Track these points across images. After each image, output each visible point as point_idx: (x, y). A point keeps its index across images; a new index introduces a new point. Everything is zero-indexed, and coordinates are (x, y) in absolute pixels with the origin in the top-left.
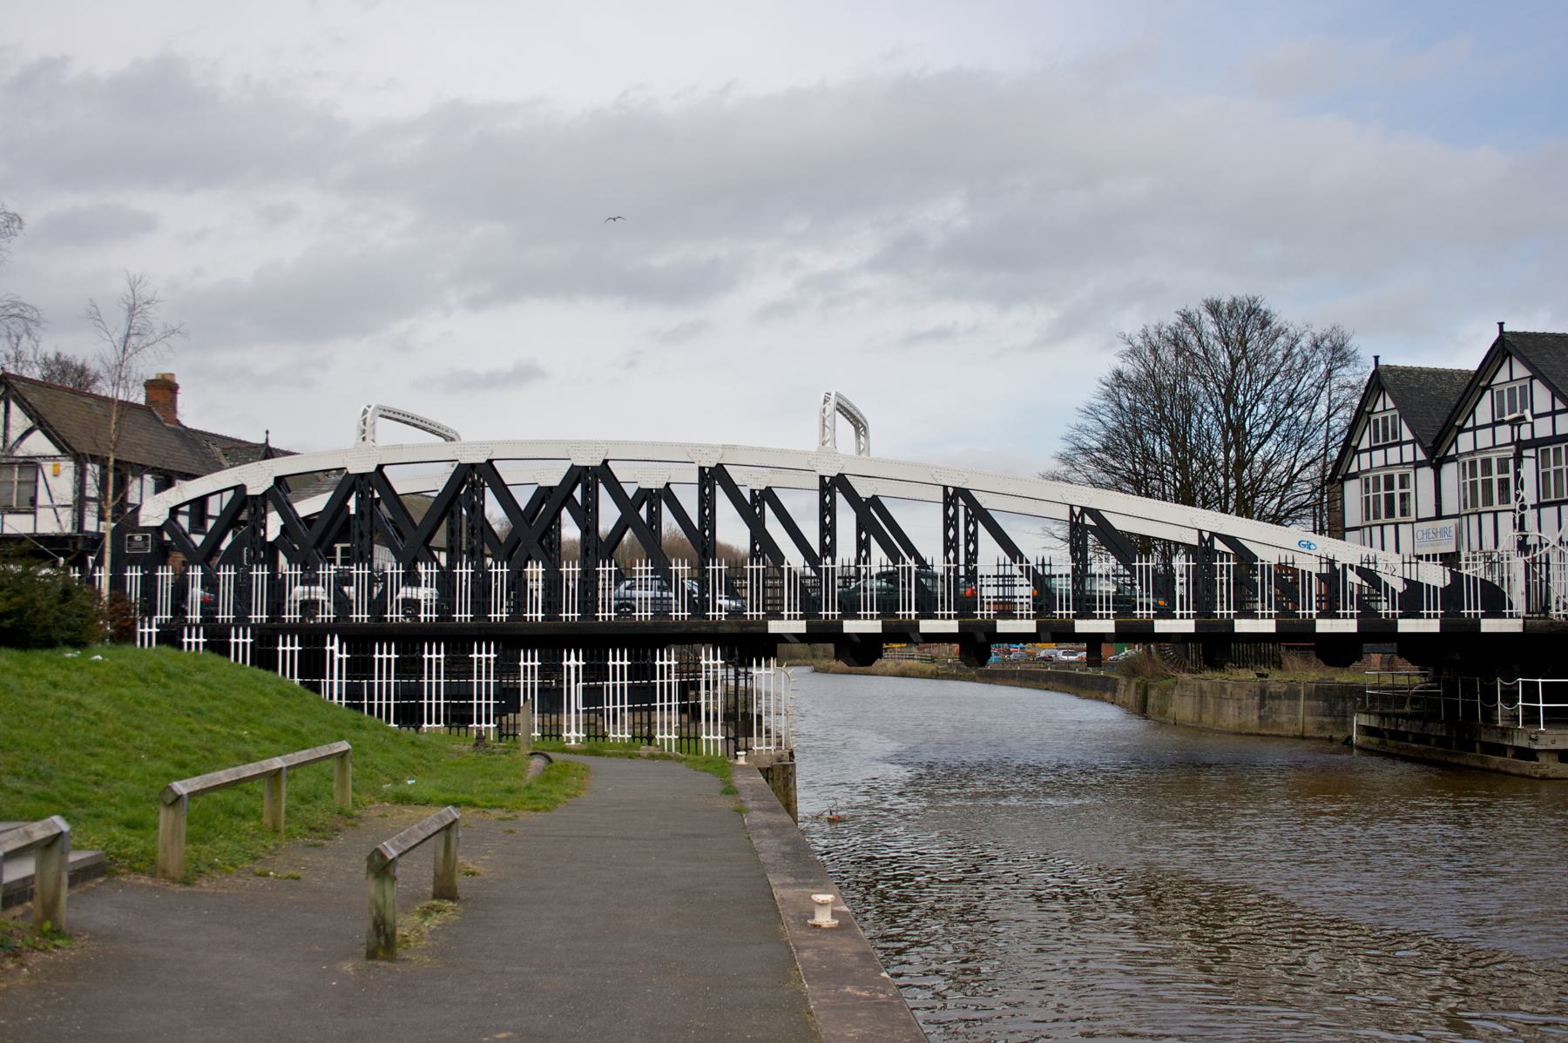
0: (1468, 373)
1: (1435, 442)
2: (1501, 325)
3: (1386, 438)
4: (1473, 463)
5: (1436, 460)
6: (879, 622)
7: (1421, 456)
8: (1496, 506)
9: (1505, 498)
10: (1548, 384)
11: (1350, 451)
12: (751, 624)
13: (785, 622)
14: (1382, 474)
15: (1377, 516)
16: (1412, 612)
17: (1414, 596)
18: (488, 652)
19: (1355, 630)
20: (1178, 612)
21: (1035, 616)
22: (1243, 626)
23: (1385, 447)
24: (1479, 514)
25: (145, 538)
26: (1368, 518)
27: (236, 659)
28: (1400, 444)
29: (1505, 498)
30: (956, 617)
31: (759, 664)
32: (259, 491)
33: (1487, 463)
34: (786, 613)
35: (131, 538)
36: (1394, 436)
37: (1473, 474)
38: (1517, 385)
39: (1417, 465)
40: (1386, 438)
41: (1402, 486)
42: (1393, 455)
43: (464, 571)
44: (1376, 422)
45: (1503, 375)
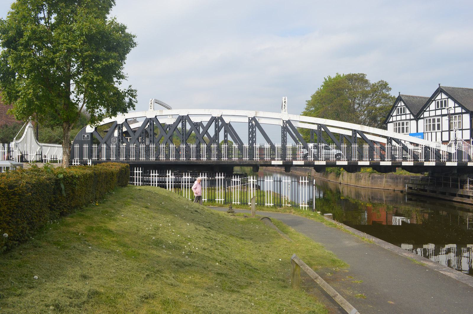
0: (427, 98)
1: (417, 114)
2: (439, 84)
3: (401, 112)
4: (430, 120)
5: (417, 118)
6: (391, 162)
7: (412, 117)
8: (436, 130)
9: (439, 129)
10: (453, 99)
11: (390, 116)
13: (408, 162)
14: (401, 122)
15: (430, 130)
16: (449, 160)
18: (139, 170)
19: (413, 165)
20: (386, 159)
21: (391, 161)
23: (401, 115)
24: (431, 133)
25: (88, 136)
26: (427, 130)
28: (406, 114)
30: (391, 161)
32: (121, 123)
33: (434, 120)
34: (276, 159)
35: (84, 136)
36: (404, 112)
37: (396, 126)
38: (443, 100)
39: (411, 120)
40: (401, 112)
41: (406, 125)
42: (403, 117)
43: (152, 146)
44: (398, 109)
45: (439, 97)
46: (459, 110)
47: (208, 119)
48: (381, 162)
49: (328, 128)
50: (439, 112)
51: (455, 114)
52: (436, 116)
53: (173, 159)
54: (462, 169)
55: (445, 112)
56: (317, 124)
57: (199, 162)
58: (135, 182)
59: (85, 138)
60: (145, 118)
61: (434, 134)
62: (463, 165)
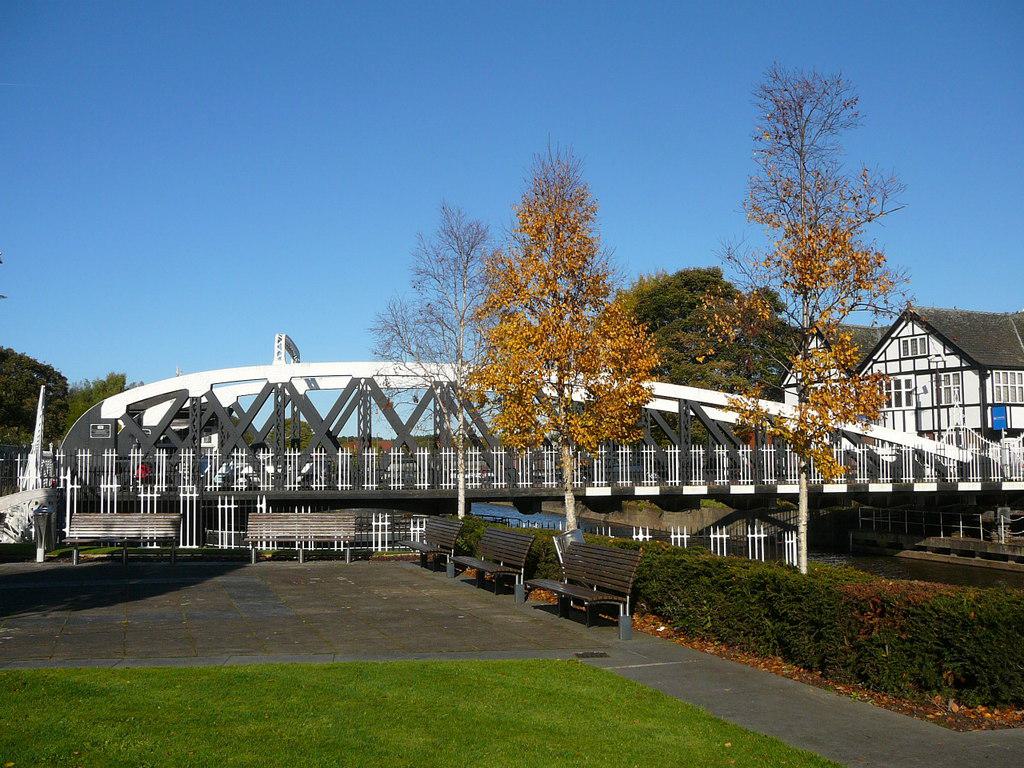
6: (658, 488)
8: (904, 407)
9: (909, 403)
12: (447, 492)
17: (963, 470)
19: (658, 493)
20: (595, 482)
22: (874, 488)
25: (106, 427)
27: (753, 556)
29: (909, 403)
31: (300, 511)
33: (898, 384)
35: (95, 427)
45: (907, 331)
46: (954, 361)
47: (258, 388)
48: (960, 484)
49: (990, 378)
50: (907, 366)
51: (945, 370)
52: (901, 373)
53: (344, 485)
54: (992, 497)
55: (922, 364)
56: (679, 400)
57: (359, 494)
58: (374, 548)
59: (97, 432)
60: (264, 383)
61: (899, 416)
62: (992, 488)
